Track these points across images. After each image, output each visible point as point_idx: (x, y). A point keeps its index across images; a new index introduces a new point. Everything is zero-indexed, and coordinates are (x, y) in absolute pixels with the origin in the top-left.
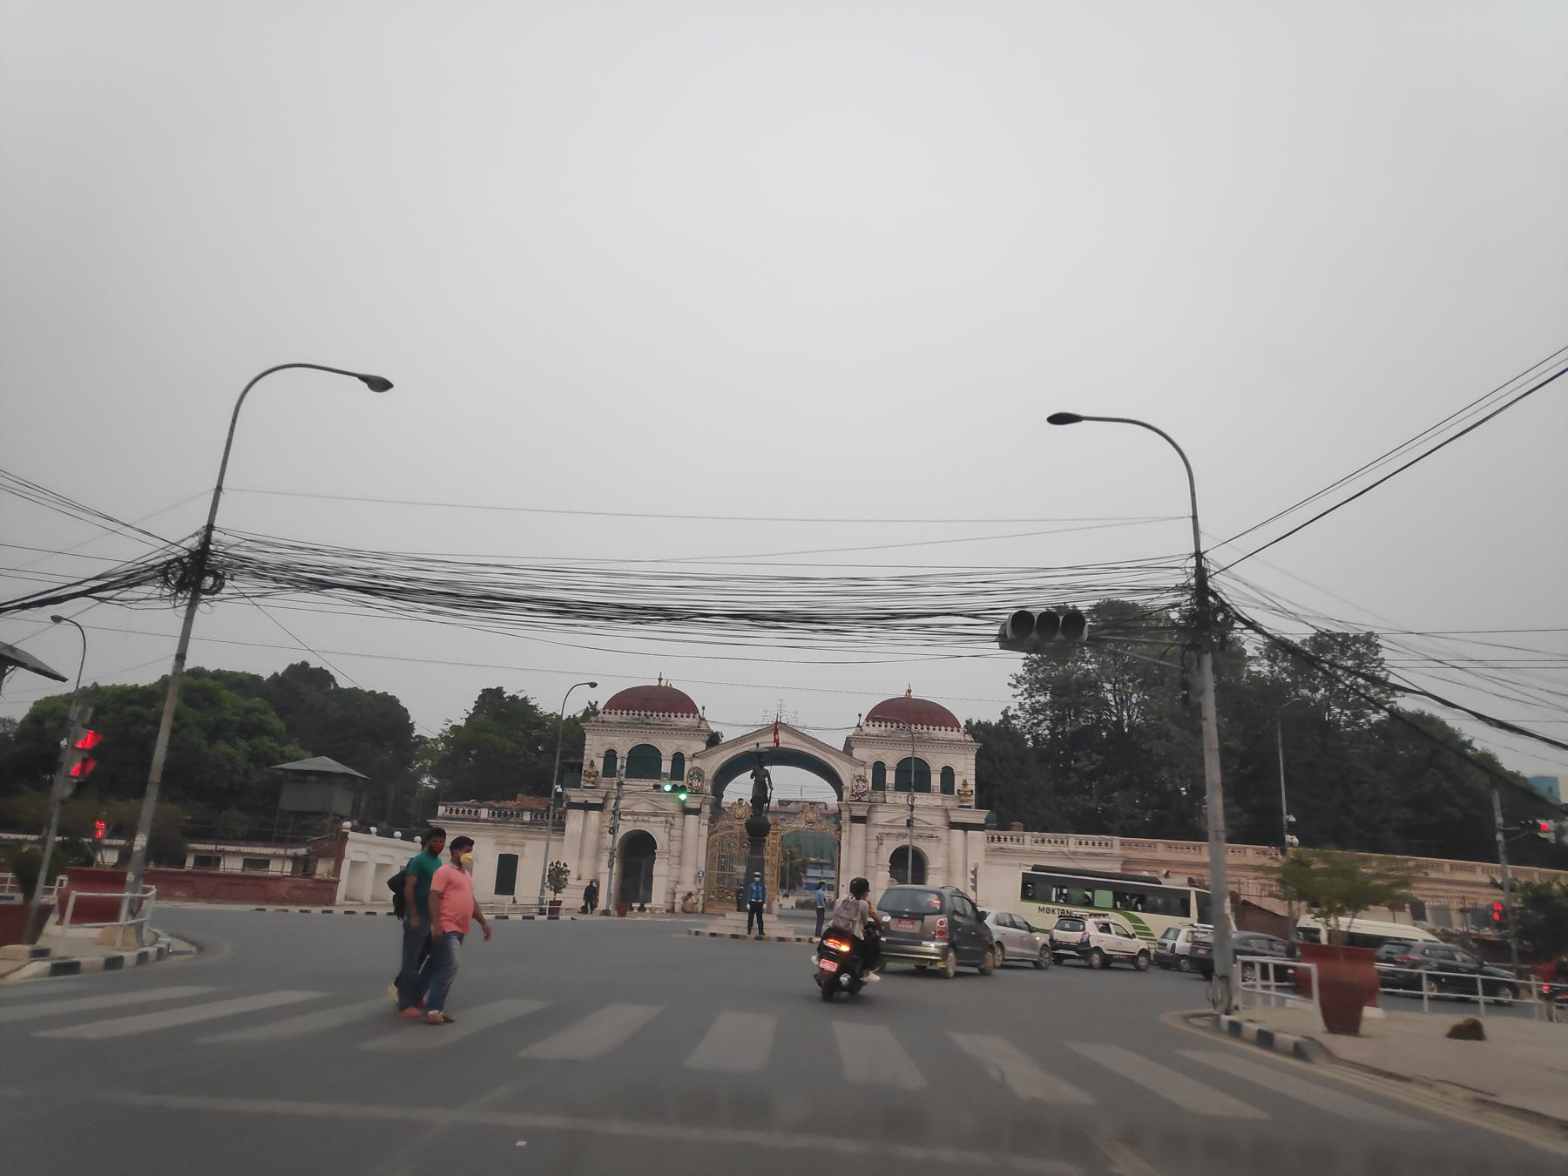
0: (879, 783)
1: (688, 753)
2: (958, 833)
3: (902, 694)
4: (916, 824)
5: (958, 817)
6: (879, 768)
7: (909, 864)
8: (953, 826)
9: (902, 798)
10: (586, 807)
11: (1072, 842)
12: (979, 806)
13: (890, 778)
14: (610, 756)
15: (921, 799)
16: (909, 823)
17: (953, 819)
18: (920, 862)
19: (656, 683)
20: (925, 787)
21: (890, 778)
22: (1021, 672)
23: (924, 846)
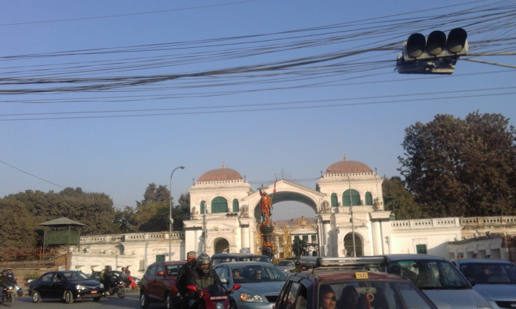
0: (335, 204)
1: (239, 198)
2: (378, 223)
3: (342, 160)
4: (354, 220)
5: (375, 216)
6: (334, 197)
7: (354, 242)
8: (373, 220)
9: (347, 209)
10: (195, 229)
11: (311, 193)
12: (386, 210)
13: (340, 200)
14: (203, 204)
15: (355, 208)
16: (351, 220)
17: (374, 217)
18: (359, 239)
19: (221, 167)
20: (359, 203)
21: (340, 200)
22: (235, 249)
23: (360, 231)
